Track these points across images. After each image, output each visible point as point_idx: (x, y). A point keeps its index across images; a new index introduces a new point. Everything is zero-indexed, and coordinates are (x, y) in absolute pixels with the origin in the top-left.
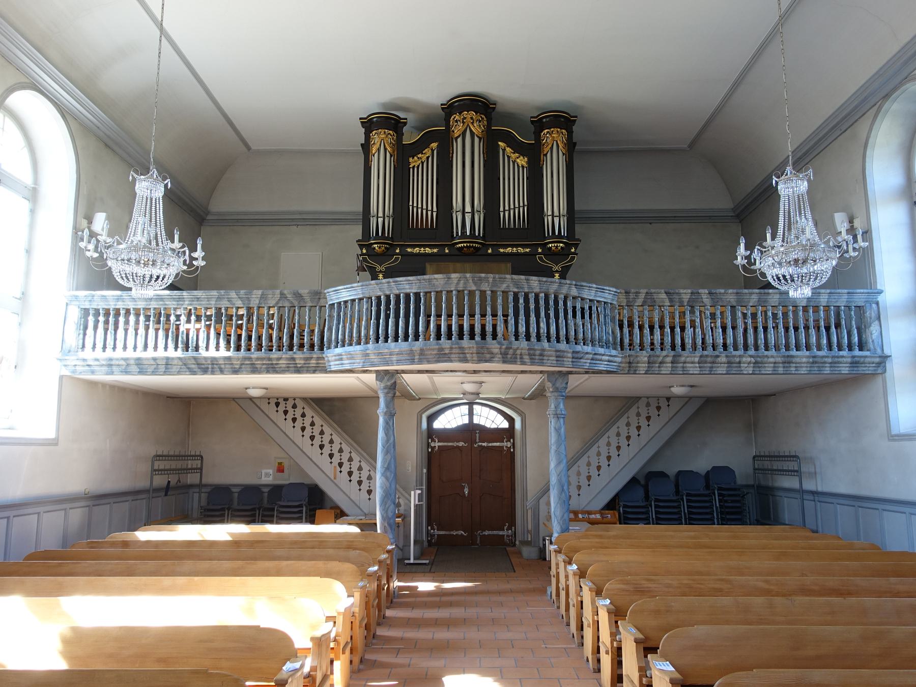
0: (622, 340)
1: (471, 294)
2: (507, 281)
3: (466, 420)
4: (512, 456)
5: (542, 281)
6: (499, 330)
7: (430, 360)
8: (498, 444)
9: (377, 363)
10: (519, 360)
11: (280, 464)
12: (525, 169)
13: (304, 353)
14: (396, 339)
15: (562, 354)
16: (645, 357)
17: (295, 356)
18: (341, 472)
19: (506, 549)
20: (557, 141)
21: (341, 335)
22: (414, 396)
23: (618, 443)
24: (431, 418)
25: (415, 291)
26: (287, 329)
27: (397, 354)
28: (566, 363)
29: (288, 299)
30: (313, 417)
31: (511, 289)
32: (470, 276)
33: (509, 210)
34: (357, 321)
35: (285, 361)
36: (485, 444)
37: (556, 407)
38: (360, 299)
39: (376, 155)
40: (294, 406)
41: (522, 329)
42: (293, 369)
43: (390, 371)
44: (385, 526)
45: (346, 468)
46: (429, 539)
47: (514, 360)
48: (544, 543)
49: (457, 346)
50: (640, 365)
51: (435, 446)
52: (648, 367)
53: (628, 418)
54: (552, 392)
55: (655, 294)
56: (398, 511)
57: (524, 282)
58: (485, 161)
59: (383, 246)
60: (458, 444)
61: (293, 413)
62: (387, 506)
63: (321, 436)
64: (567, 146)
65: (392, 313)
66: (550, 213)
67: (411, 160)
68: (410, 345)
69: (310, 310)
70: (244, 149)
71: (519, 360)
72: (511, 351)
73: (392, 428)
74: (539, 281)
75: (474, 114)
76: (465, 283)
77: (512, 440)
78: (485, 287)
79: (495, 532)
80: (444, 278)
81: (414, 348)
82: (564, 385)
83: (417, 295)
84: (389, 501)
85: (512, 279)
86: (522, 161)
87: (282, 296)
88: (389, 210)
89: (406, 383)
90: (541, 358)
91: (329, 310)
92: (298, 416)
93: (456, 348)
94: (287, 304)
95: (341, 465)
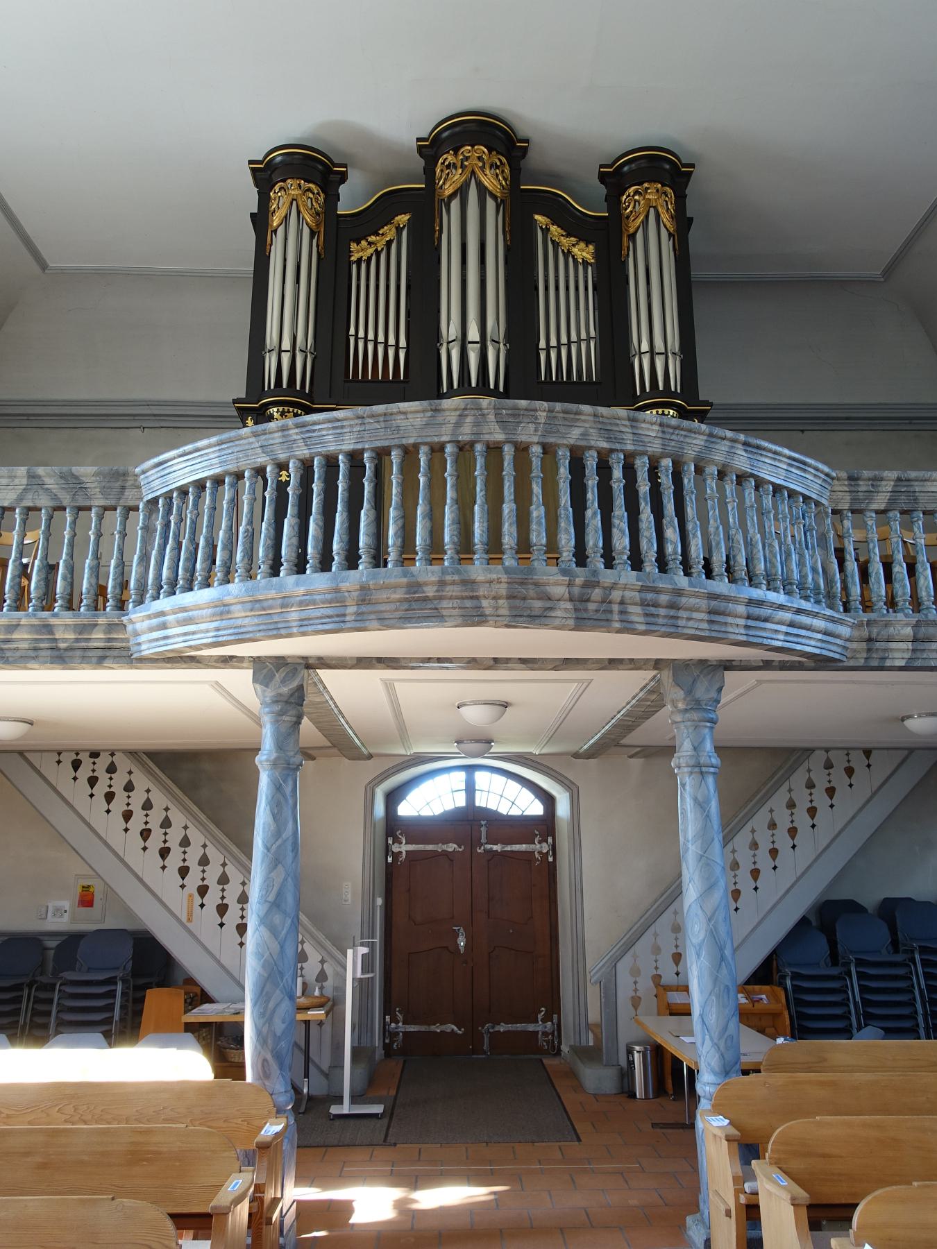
0: (845, 588)
1: (494, 450)
2: (584, 421)
3: (461, 801)
4: (550, 871)
5: (669, 426)
6: (563, 542)
7: (386, 615)
8: (523, 847)
9: (250, 629)
10: (616, 617)
11: (86, 888)
12: (590, 268)
13: (79, 616)
14: (300, 567)
15: (722, 605)
16: (907, 625)
17: (53, 621)
18: (202, 906)
19: (541, 1060)
20: (655, 208)
21: (169, 568)
22: (357, 748)
23: (773, 842)
24: (393, 798)
25: (351, 447)
26: (41, 560)
27: (301, 603)
28: (730, 629)
29: (47, 489)
30: (148, 791)
31: (593, 443)
32: (490, 404)
33: (559, 347)
34: (207, 532)
35: (30, 633)
36: (496, 848)
37: (695, 749)
38: (218, 481)
39: (281, 231)
40: (112, 769)
41: (621, 541)
42: (49, 653)
43: (289, 661)
44: (265, 1060)
45: (212, 899)
46: (387, 1041)
47: (603, 617)
48: (631, 1058)
49: (456, 578)
50: (893, 645)
51: (401, 852)
52: (914, 650)
53: (790, 790)
54: (686, 711)
55: (916, 483)
56: (321, 988)
57: (625, 426)
58: (507, 249)
59: (291, 409)
60: (444, 847)
61: (108, 782)
62: (271, 1005)
63: (163, 831)
64: (675, 219)
65: (292, 505)
66: (645, 347)
67: (353, 246)
68: (335, 578)
69: (101, 518)
70: (36, 269)
71: (616, 617)
72: (597, 594)
73: (291, 801)
74: (661, 425)
75: (486, 150)
76: (477, 424)
77: (550, 840)
78: (528, 434)
79: (519, 1027)
80: (424, 411)
81: (344, 586)
82: (713, 694)
83: (355, 458)
84: (278, 992)
85: (595, 416)
86: (584, 252)
87: (35, 481)
88: (305, 338)
89: (335, 703)
90: (672, 613)
91: (145, 515)
92: (118, 788)
93: (454, 583)
94: (44, 501)
95: (203, 891)
